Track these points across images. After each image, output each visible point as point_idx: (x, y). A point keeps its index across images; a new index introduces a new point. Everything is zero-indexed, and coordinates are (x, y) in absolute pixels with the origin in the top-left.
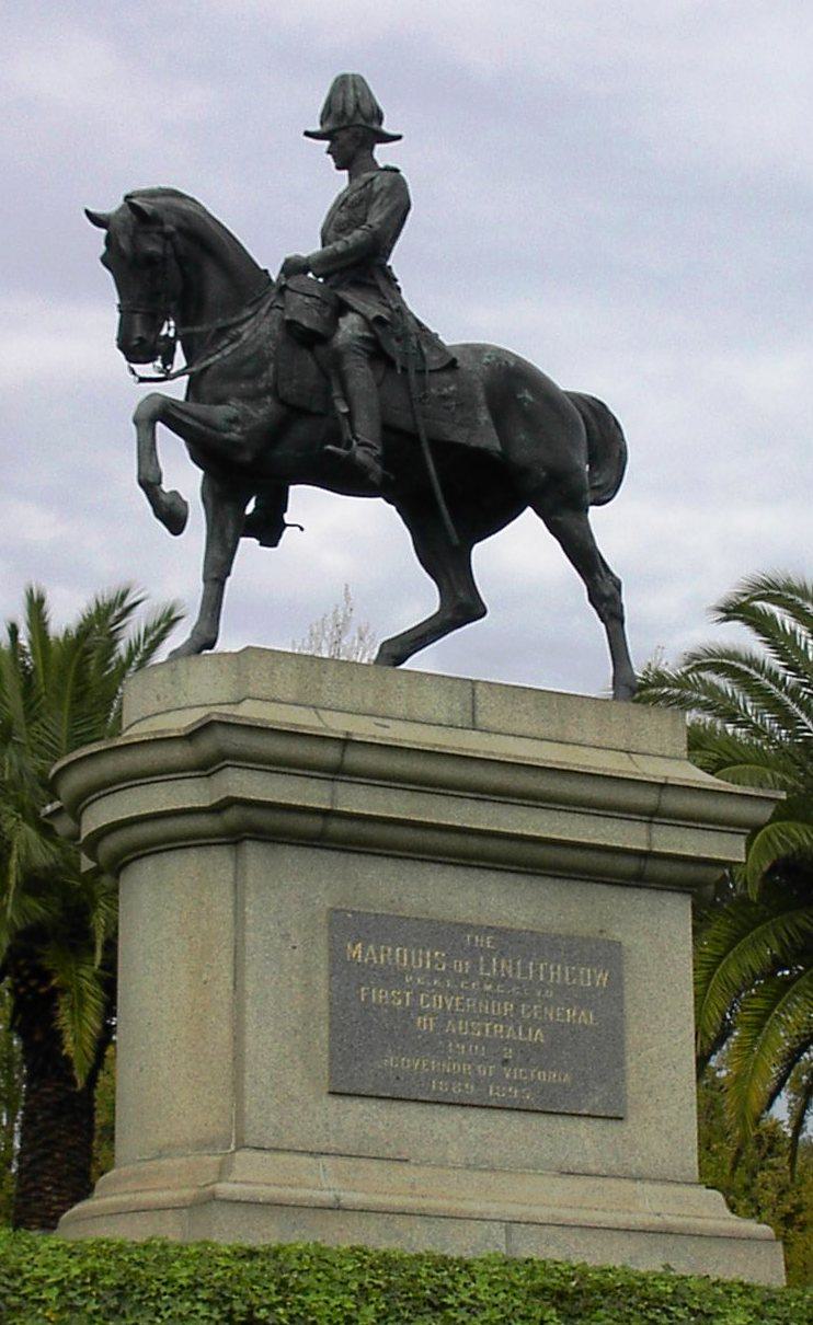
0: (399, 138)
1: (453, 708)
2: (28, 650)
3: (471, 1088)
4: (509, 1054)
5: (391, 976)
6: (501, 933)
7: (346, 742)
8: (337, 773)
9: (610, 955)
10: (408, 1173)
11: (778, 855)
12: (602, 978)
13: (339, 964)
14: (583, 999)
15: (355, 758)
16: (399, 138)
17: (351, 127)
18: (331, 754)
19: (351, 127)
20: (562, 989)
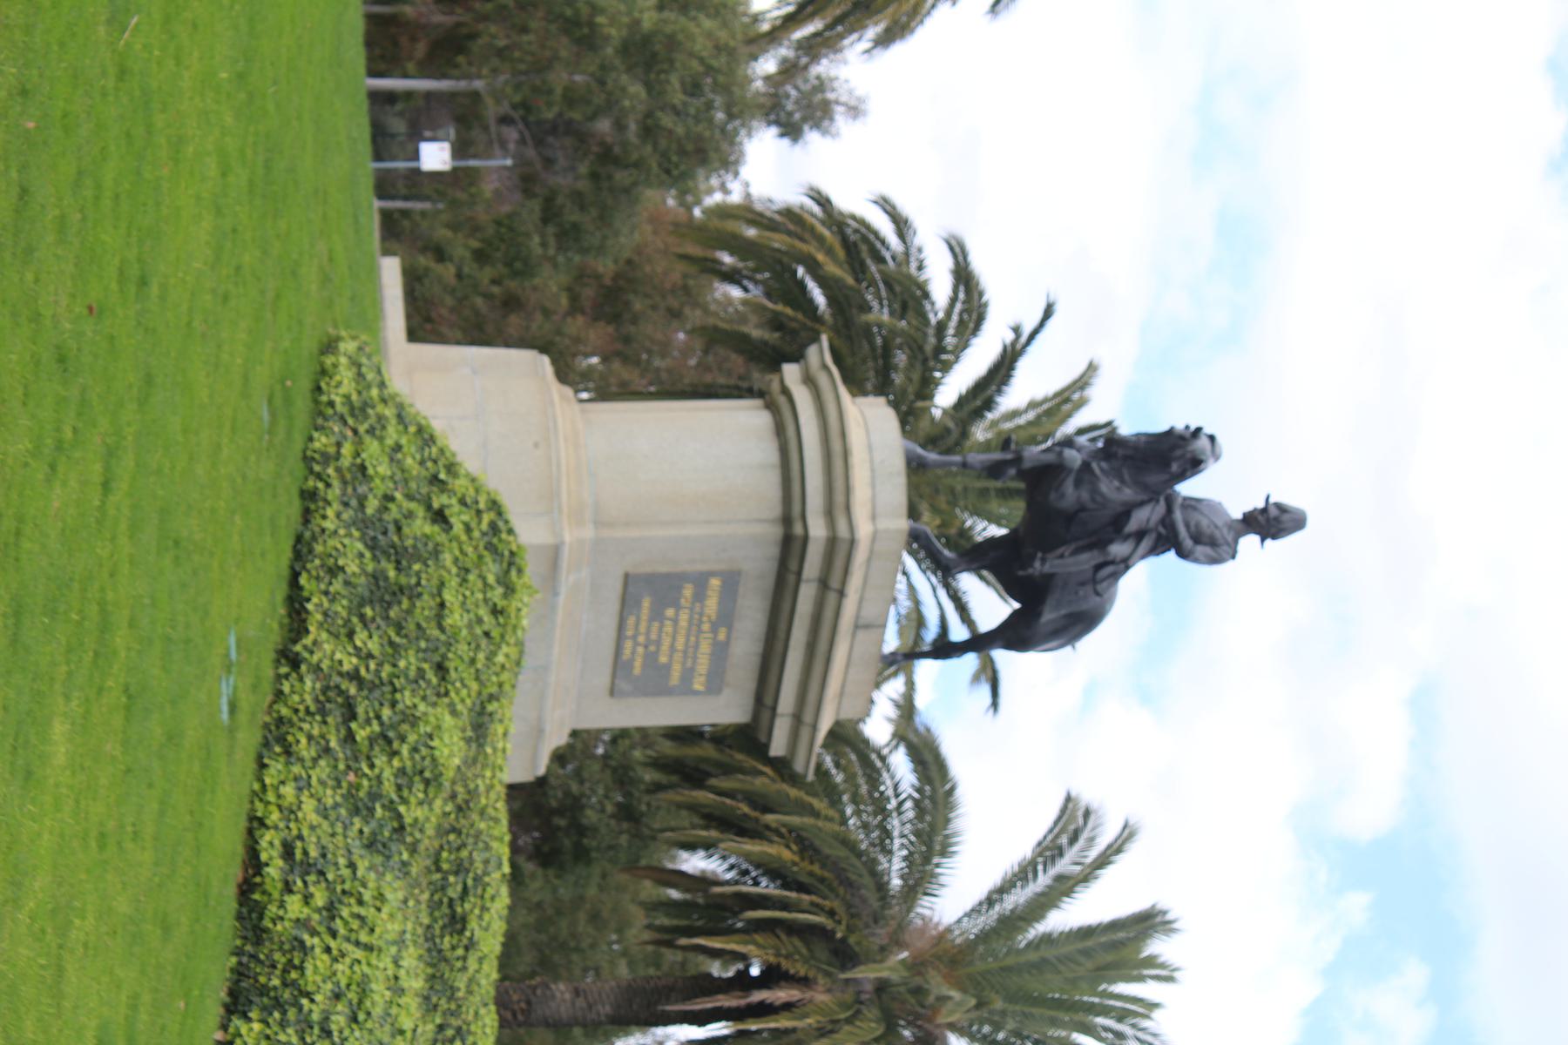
0: (1092, 368)
1: (869, 613)
2: (828, 317)
3: (629, 633)
4: (652, 648)
5: (700, 596)
6: (727, 643)
7: (841, 594)
8: (824, 583)
9: (715, 685)
10: (681, 250)
11: (748, 196)
12: (698, 687)
13: (700, 581)
14: (688, 675)
15: (832, 598)
16: (1092, 368)
17: (1272, 522)
18: (835, 583)
19: (1272, 522)
20: (692, 670)
